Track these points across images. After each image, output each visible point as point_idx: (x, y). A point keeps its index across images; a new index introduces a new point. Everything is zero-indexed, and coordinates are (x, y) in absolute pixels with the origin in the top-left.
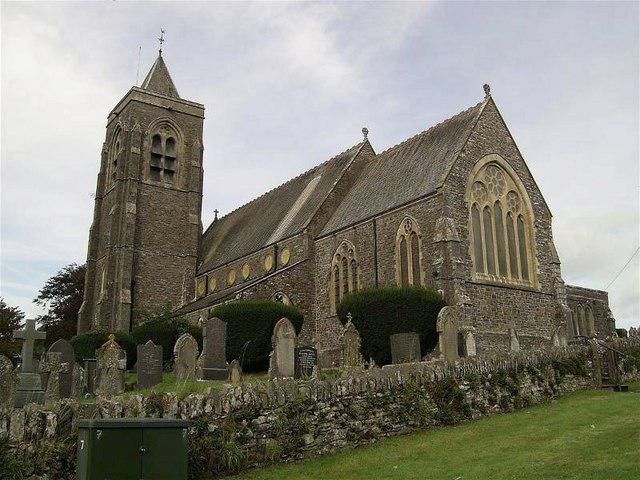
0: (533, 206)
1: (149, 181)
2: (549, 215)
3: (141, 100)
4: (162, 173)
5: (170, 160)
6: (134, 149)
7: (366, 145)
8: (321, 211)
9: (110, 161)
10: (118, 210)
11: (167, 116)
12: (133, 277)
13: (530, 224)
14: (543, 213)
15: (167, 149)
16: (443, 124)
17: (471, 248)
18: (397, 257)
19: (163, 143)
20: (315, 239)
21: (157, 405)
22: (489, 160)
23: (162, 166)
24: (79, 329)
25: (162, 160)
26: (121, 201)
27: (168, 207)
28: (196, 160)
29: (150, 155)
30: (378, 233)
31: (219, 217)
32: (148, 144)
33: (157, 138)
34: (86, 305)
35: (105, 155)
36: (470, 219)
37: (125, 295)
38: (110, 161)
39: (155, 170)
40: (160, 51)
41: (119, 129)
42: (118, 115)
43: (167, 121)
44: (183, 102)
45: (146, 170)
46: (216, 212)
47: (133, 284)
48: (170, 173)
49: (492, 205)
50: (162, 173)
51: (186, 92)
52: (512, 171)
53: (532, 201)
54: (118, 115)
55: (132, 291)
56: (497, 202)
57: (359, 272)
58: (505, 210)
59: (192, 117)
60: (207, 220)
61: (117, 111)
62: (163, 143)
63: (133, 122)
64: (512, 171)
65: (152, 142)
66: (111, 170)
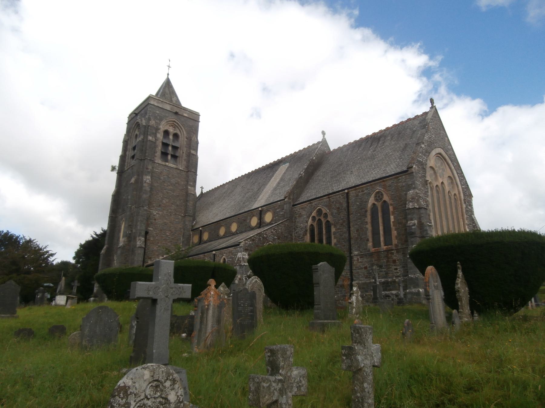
0: (462, 188)
1: (160, 162)
2: (470, 196)
3: (156, 104)
4: (169, 157)
5: (175, 148)
6: (150, 138)
7: (324, 143)
8: (303, 182)
9: (130, 147)
10: (137, 181)
11: (173, 118)
12: (146, 228)
13: (461, 201)
14: (468, 195)
15: (173, 141)
16: (378, 133)
17: (432, 214)
18: (369, 219)
19: (171, 137)
20: (294, 205)
21: (459, 278)
22: (437, 152)
23: (170, 151)
24: (100, 268)
25: (170, 148)
26: (140, 174)
27: (173, 181)
28: (194, 150)
29: (161, 144)
30: (350, 201)
31: (204, 191)
32: (160, 136)
33: (166, 133)
34: (107, 248)
35: (126, 143)
36: (429, 193)
37: (140, 242)
38: (130, 147)
39: (164, 154)
40: (168, 74)
41: (138, 125)
42: (136, 114)
43: (174, 121)
44: (185, 109)
45: (159, 154)
46: (202, 188)
47: (147, 233)
48: (174, 157)
49: (440, 185)
50: (169, 157)
51: (187, 101)
52: (450, 162)
53: (462, 185)
54: (136, 114)
55: (146, 238)
56: (442, 183)
57: (333, 230)
58: (447, 188)
59: (190, 121)
60: (198, 193)
61: (136, 112)
62: (171, 137)
63: (149, 119)
64: (450, 162)
65: (160, 135)
66: (130, 153)
